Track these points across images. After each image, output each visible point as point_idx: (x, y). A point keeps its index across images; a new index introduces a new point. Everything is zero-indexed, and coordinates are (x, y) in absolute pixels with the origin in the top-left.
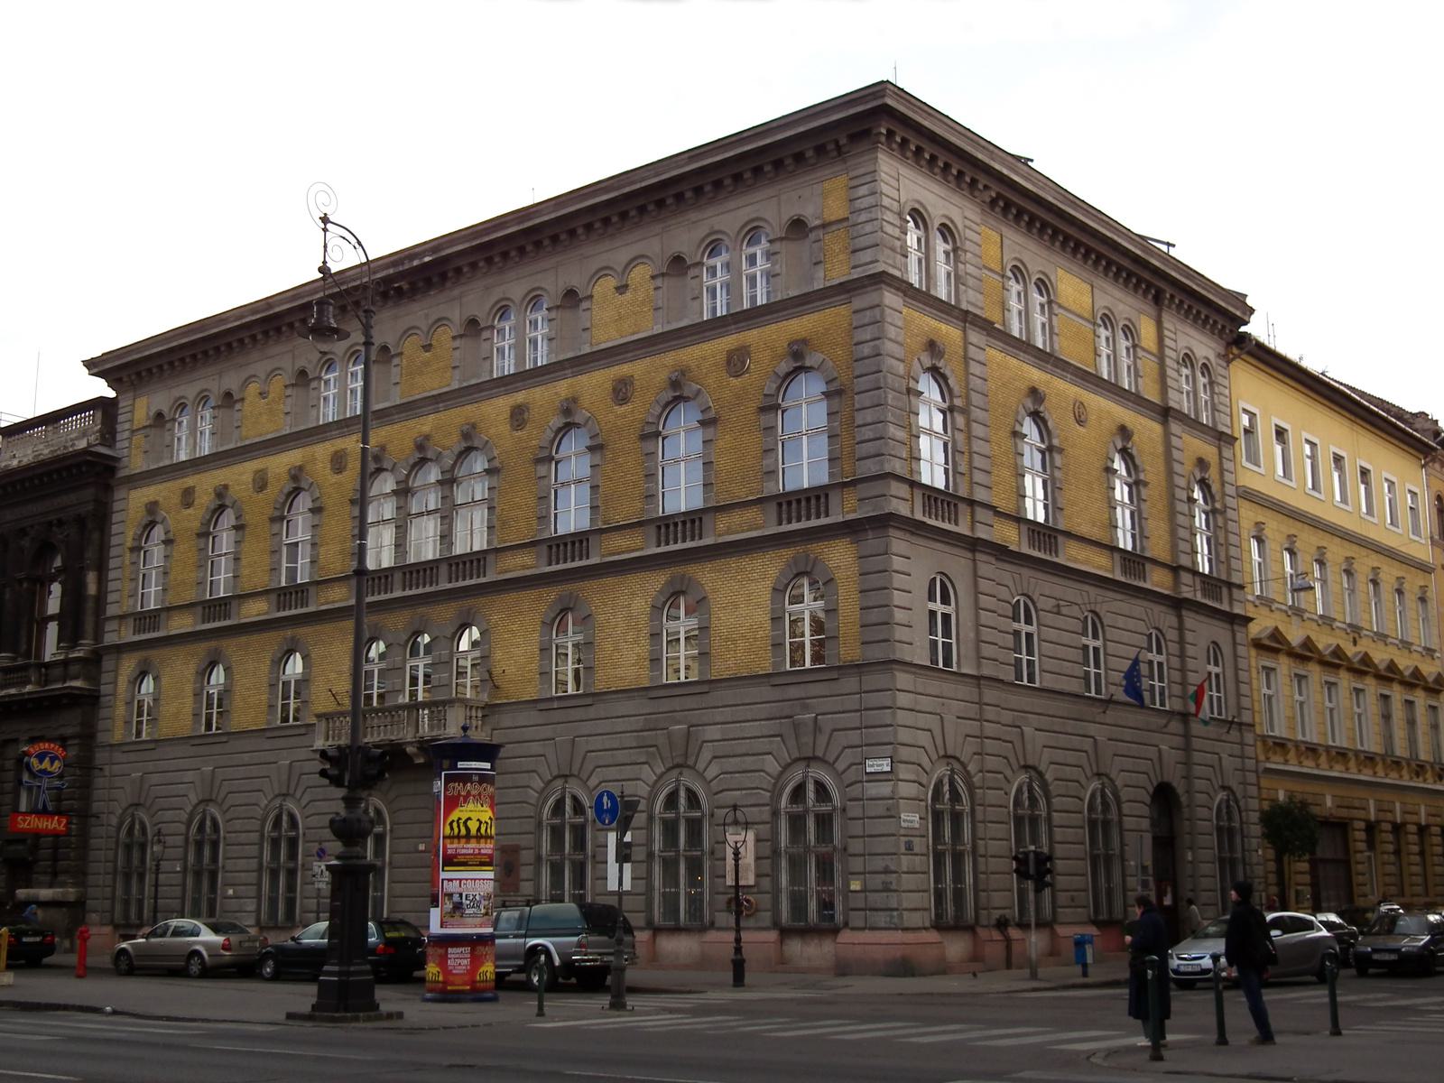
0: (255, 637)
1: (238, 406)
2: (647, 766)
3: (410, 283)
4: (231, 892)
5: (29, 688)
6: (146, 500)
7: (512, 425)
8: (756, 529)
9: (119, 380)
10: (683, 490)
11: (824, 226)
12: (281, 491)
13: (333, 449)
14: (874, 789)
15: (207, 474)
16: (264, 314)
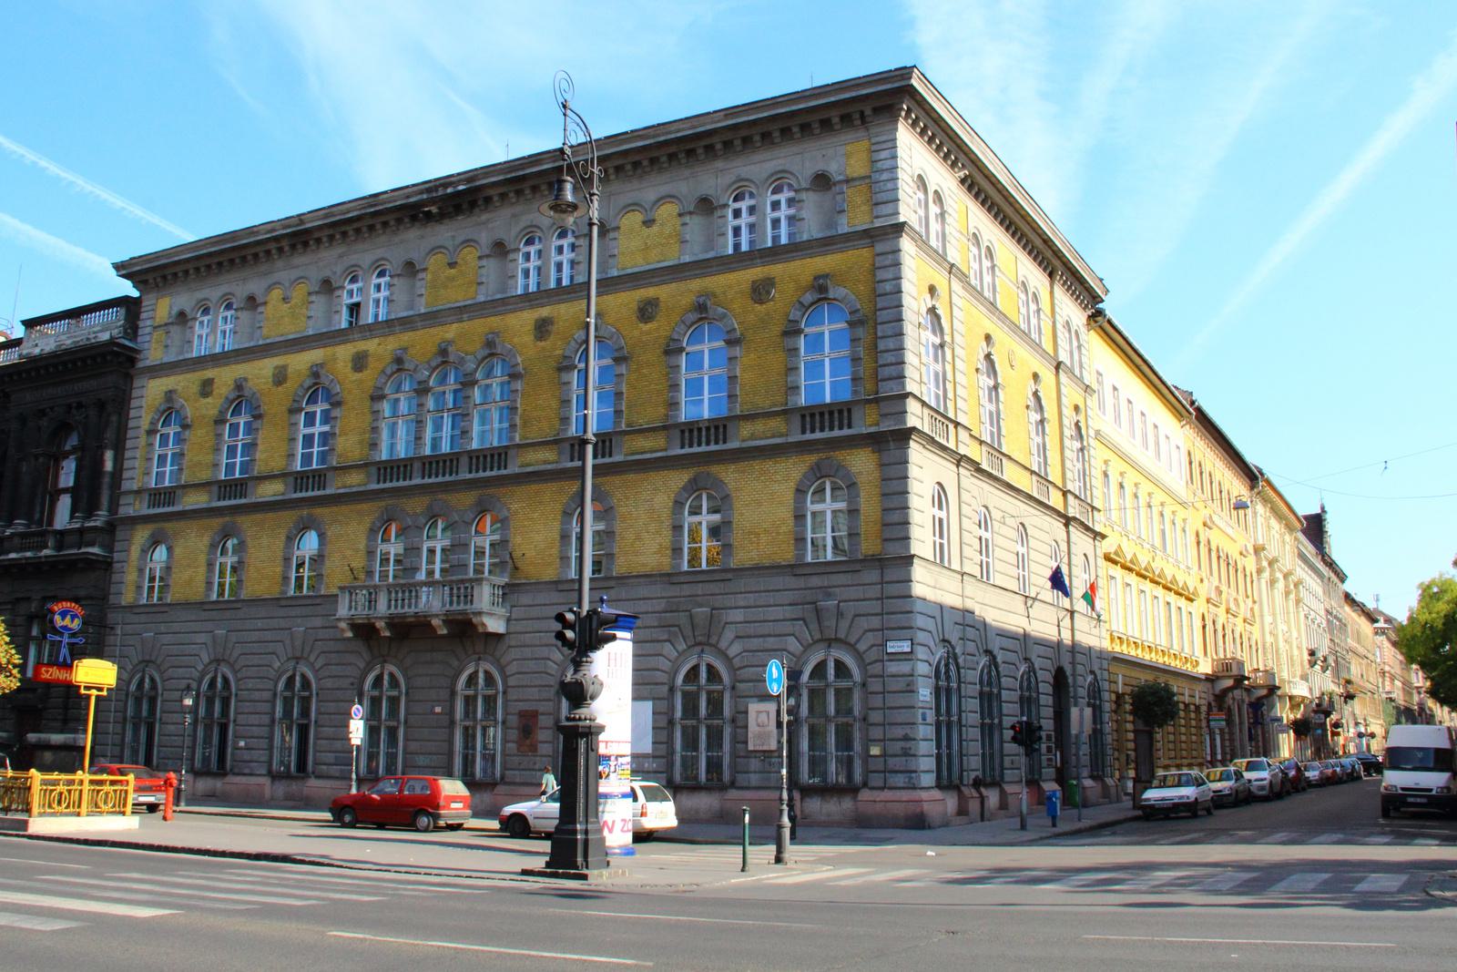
0: (270, 515)
1: (260, 309)
2: (667, 643)
3: (439, 208)
4: (242, 744)
5: (46, 552)
6: (165, 389)
7: (535, 337)
8: (779, 437)
9: (145, 282)
10: (706, 401)
11: (847, 181)
12: (302, 386)
13: (355, 350)
14: (893, 668)
15: (227, 368)
16: (294, 229)
